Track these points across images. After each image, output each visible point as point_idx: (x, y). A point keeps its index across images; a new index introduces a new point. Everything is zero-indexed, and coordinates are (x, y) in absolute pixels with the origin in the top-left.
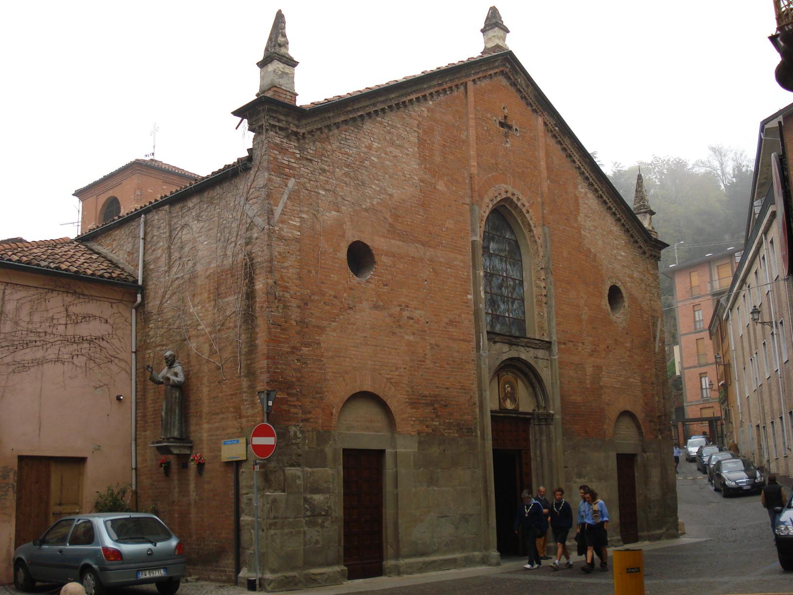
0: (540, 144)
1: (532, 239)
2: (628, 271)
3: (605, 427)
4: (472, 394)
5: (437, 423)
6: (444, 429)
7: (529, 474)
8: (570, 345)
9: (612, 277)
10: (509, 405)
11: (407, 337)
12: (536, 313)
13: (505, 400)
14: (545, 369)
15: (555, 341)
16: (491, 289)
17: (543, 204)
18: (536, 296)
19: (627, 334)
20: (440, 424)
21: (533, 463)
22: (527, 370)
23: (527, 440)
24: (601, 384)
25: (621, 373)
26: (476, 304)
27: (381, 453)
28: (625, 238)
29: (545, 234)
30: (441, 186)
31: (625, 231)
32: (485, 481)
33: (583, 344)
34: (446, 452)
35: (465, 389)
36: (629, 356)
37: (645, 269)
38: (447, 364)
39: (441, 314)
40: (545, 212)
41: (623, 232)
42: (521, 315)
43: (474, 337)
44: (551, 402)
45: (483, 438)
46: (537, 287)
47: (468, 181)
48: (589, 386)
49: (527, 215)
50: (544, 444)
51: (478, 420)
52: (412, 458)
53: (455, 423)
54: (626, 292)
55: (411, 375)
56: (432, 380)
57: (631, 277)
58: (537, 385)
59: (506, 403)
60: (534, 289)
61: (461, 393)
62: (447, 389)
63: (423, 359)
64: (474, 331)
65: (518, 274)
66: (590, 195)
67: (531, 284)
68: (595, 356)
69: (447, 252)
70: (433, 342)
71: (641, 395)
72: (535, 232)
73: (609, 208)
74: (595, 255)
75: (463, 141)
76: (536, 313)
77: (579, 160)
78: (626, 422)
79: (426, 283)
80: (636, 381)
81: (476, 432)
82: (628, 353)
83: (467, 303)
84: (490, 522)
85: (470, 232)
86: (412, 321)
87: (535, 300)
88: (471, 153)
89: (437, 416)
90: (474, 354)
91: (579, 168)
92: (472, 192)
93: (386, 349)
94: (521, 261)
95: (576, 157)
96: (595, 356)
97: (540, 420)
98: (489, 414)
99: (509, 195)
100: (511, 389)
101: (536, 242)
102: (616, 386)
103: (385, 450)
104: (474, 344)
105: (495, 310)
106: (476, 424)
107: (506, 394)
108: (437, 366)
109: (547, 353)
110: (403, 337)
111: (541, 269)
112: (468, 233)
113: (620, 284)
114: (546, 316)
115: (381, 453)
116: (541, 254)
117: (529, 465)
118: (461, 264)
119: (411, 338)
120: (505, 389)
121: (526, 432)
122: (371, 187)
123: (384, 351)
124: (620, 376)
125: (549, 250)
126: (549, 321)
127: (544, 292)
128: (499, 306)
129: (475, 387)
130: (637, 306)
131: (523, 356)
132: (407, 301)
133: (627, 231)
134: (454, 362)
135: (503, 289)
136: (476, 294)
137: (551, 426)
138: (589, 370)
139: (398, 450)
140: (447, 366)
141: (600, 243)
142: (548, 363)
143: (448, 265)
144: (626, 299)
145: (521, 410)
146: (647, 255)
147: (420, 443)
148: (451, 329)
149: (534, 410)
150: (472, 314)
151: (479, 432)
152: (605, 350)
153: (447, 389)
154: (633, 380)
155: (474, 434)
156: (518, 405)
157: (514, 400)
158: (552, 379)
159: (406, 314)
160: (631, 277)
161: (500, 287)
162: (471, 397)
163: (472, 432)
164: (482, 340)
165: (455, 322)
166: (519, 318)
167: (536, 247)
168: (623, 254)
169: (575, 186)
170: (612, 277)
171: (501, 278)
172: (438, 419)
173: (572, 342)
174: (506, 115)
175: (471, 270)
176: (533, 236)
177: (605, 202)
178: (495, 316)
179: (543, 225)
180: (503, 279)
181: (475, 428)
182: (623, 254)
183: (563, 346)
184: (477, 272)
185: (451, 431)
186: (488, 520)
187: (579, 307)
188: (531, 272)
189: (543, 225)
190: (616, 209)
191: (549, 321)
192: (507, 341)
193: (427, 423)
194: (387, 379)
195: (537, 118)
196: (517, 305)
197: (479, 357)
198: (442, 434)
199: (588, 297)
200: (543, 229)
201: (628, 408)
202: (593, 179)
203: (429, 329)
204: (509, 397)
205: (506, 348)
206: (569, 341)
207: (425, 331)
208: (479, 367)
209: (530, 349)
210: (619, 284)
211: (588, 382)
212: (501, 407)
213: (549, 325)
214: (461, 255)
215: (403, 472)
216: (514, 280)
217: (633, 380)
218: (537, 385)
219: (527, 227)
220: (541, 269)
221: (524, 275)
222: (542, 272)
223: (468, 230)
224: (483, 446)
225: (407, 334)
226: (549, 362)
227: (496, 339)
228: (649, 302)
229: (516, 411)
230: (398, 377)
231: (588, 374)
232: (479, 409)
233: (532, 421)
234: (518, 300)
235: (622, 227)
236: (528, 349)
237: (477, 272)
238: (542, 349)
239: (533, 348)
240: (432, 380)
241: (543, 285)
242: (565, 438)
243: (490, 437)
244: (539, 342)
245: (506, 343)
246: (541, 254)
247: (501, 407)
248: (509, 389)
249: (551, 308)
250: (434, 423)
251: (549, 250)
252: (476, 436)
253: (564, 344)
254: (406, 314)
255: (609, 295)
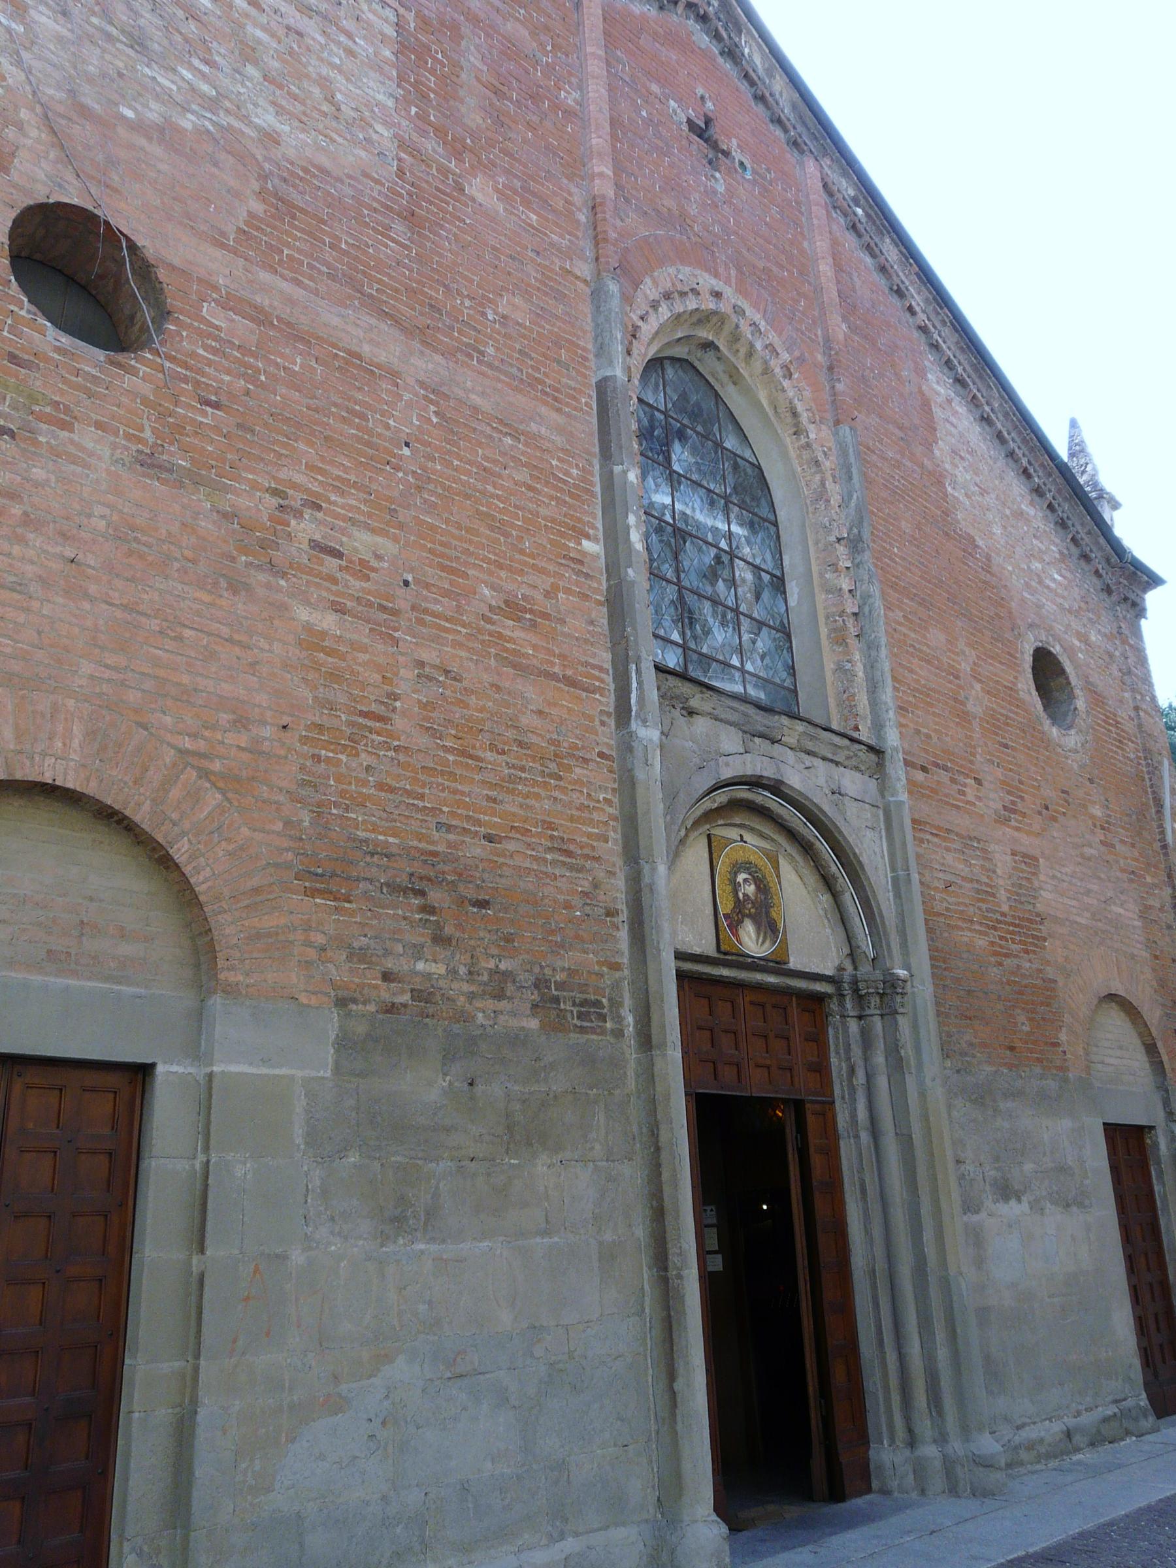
0: (815, 221)
1: (806, 455)
2: (1076, 625)
3: (1063, 1037)
4: (601, 875)
5: (441, 969)
6: (471, 997)
7: (834, 1186)
8: (944, 776)
9: (1038, 626)
10: (751, 941)
11: (303, 614)
12: (829, 666)
13: (735, 926)
14: (869, 833)
15: (896, 749)
16: (677, 571)
17: (831, 368)
18: (827, 617)
19: (1091, 781)
20: (453, 972)
21: (847, 1150)
22: (810, 832)
23: (821, 1069)
24: (1040, 907)
25: (1090, 886)
26: (613, 568)
27: (142, 1073)
28: (1057, 541)
29: (843, 452)
30: (479, 189)
31: (1056, 523)
32: (659, 1214)
33: (979, 782)
34: (479, 1088)
35: (569, 853)
36: (1102, 842)
37: (1114, 632)
38: (492, 747)
39: (471, 572)
40: (840, 387)
41: (1052, 526)
42: (784, 675)
43: (609, 679)
44: (895, 940)
45: (646, 1041)
46: (828, 592)
47: (583, 218)
48: (1005, 908)
49: (786, 383)
50: (882, 1082)
51: (626, 972)
52: (300, 1106)
53: (522, 977)
54: (1078, 676)
55: (317, 758)
56: (422, 797)
57: (1084, 638)
58: (843, 881)
59: (741, 932)
60: (820, 597)
61: (554, 863)
62: (489, 838)
63: (381, 710)
64: (605, 657)
65: (768, 556)
66: (961, 408)
67: (810, 582)
68: (1013, 823)
69: (499, 385)
70: (429, 655)
71: (1144, 954)
72: (812, 436)
73: (1011, 455)
74: (989, 558)
75: (569, 113)
76: (829, 666)
77: (924, 311)
78: (1115, 1023)
79: (406, 451)
80: (1130, 915)
81: (619, 1019)
82: (1100, 835)
83: (581, 562)
84: (678, 1385)
85: (591, 356)
86: (332, 563)
87: (824, 631)
88: (594, 142)
89: (440, 939)
90: (606, 737)
91: (923, 329)
92: (597, 244)
93: (188, 633)
94: (775, 524)
95: (917, 298)
96: (1013, 823)
97: (860, 999)
98: (669, 966)
99: (724, 307)
100: (758, 888)
101: (817, 463)
102: (1079, 919)
103: (153, 1066)
104: (609, 701)
105: (695, 637)
106: (616, 986)
107: (739, 905)
108: (446, 749)
109: (872, 785)
110: (284, 607)
111: (839, 540)
112: (586, 359)
113: (1058, 648)
114: (861, 674)
115: (142, 1073)
116: (835, 500)
117: (832, 1153)
118: (559, 440)
119: (328, 621)
120: (735, 887)
121: (818, 1039)
122: (174, 70)
123: (179, 638)
124: (1088, 892)
125: (857, 486)
126: (873, 688)
127: (851, 607)
128: (707, 632)
129: (612, 848)
130: (1108, 717)
131: (794, 780)
132: (315, 487)
133: (1062, 524)
134: (521, 744)
135: (720, 583)
136: (614, 537)
137: (899, 1017)
138: (1003, 862)
139: (215, 1069)
140: (489, 755)
141: (997, 530)
142: (876, 816)
143: (501, 422)
144: (1078, 692)
145: (794, 963)
146: (1115, 597)
147: (344, 1044)
148: (508, 627)
149: (841, 969)
150: (599, 603)
151: (630, 1019)
152: (1040, 813)
153: (489, 838)
154: (1121, 911)
155: (609, 1025)
156: (784, 947)
157: (769, 927)
158: (893, 869)
159: (305, 528)
160: (1084, 638)
161: (711, 575)
162: (596, 885)
163: (603, 1018)
164: (634, 685)
165: (531, 611)
166: (777, 680)
167: (818, 477)
168: (1056, 576)
169: (921, 373)
170: (1038, 626)
171: (713, 552)
172: (443, 953)
173: (945, 768)
174: (710, 114)
175: (597, 467)
176: (808, 446)
177: (999, 436)
178: (695, 657)
179: (837, 422)
180: (718, 559)
181: (615, 1004)
182: (1056, 576)
183: (920, 776)
184: (617, 469)
185: (503, 1005)
186: (672, 1376)
187: (957, 677)
188: (806, 551)
189: (837, 422)
190: (1029, 462)
191: (873, 688)
192: (734, 717)
193: (390, 964)
194: (183, 752)
195: (802, 164)
196: (769, 643)
197: (627, 746)
198: (464, 1017)
199: (978, 657)
200: (836, 434)
201: (1118, 988)
202: (964, 370)
203: (413, 608)
204: (750, 916)
205: (730, 741)
206: (937, 765)
207: (395, 613)
208: (628, 784)
209: (818, 762)
210: (1056, 649)
211: (1002, 895)
212: (723, 947)
213: (874, 703)
214: (558, 410)
215: (239, 1171)
216: (756, 569)
217: (1121, 911)
218: (843, 881)
219: (789, 420)
220: (839, 540)
221: (786, 563)
222: (841, 550)
223: (584, 349)
224: (648, 1075)
225: (307, 603)
226: (881, 813)
227: (694, 703)
228: (1133, 714)
229: (776, 964)
230: (245, 756)
231: (999, 871)
232: (631, 930)
233: (834, 1006)
234: (769, 626)
235: (1048, 512)
236: (809, 761)
237: (617, 469)
238: (857, 768)
239: (824, 759)
240: (422, 797)
241: (846, 585)
242: (948, 1063)
243: (674, 1035)
244: (846, 742)
245: (731, 724)
246: (835, 500)
247: (723, 947)
248: (751, 889)
249: (878, 648)
250: (420, 966)
251: (857, 486)
252: (619, 1033)
253: (924, 769)
254: (305, 528)
255: (1034, 668)
